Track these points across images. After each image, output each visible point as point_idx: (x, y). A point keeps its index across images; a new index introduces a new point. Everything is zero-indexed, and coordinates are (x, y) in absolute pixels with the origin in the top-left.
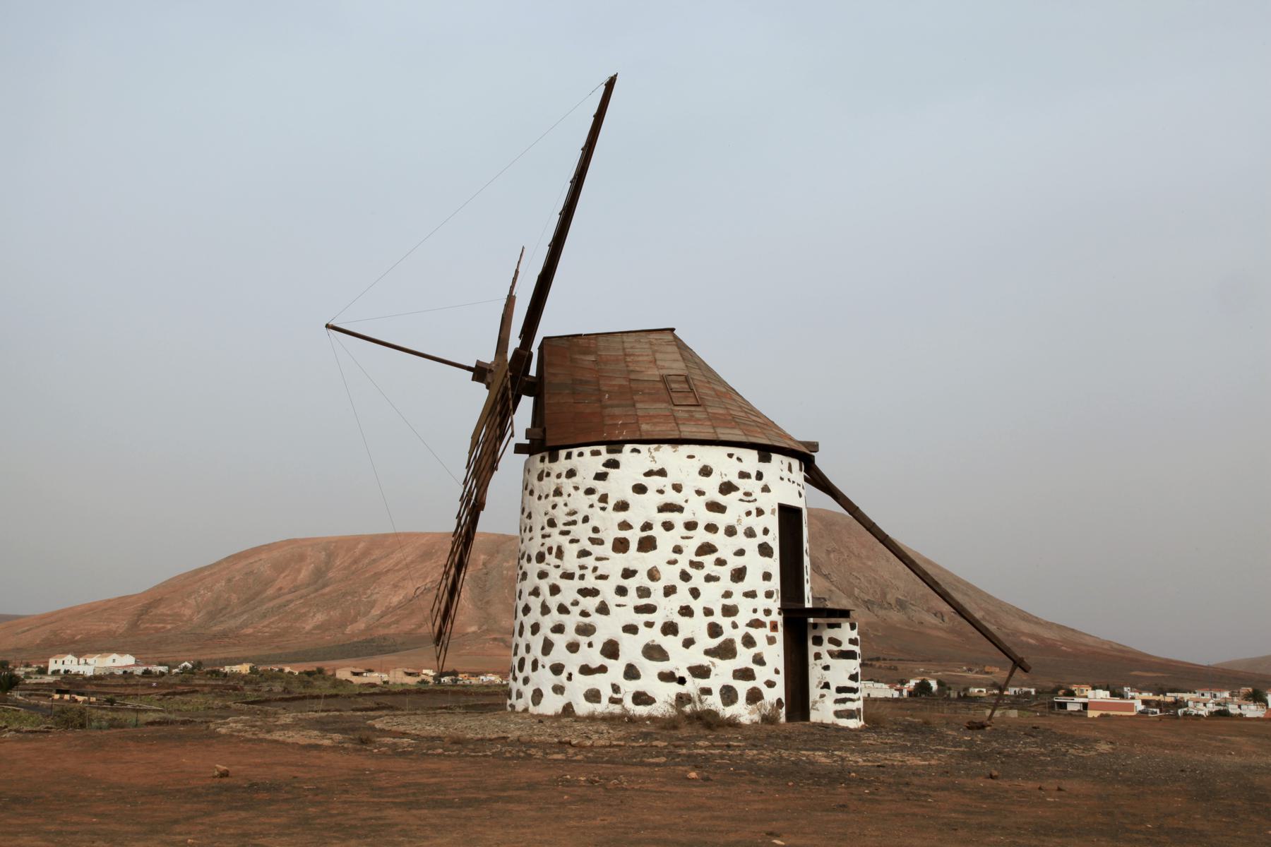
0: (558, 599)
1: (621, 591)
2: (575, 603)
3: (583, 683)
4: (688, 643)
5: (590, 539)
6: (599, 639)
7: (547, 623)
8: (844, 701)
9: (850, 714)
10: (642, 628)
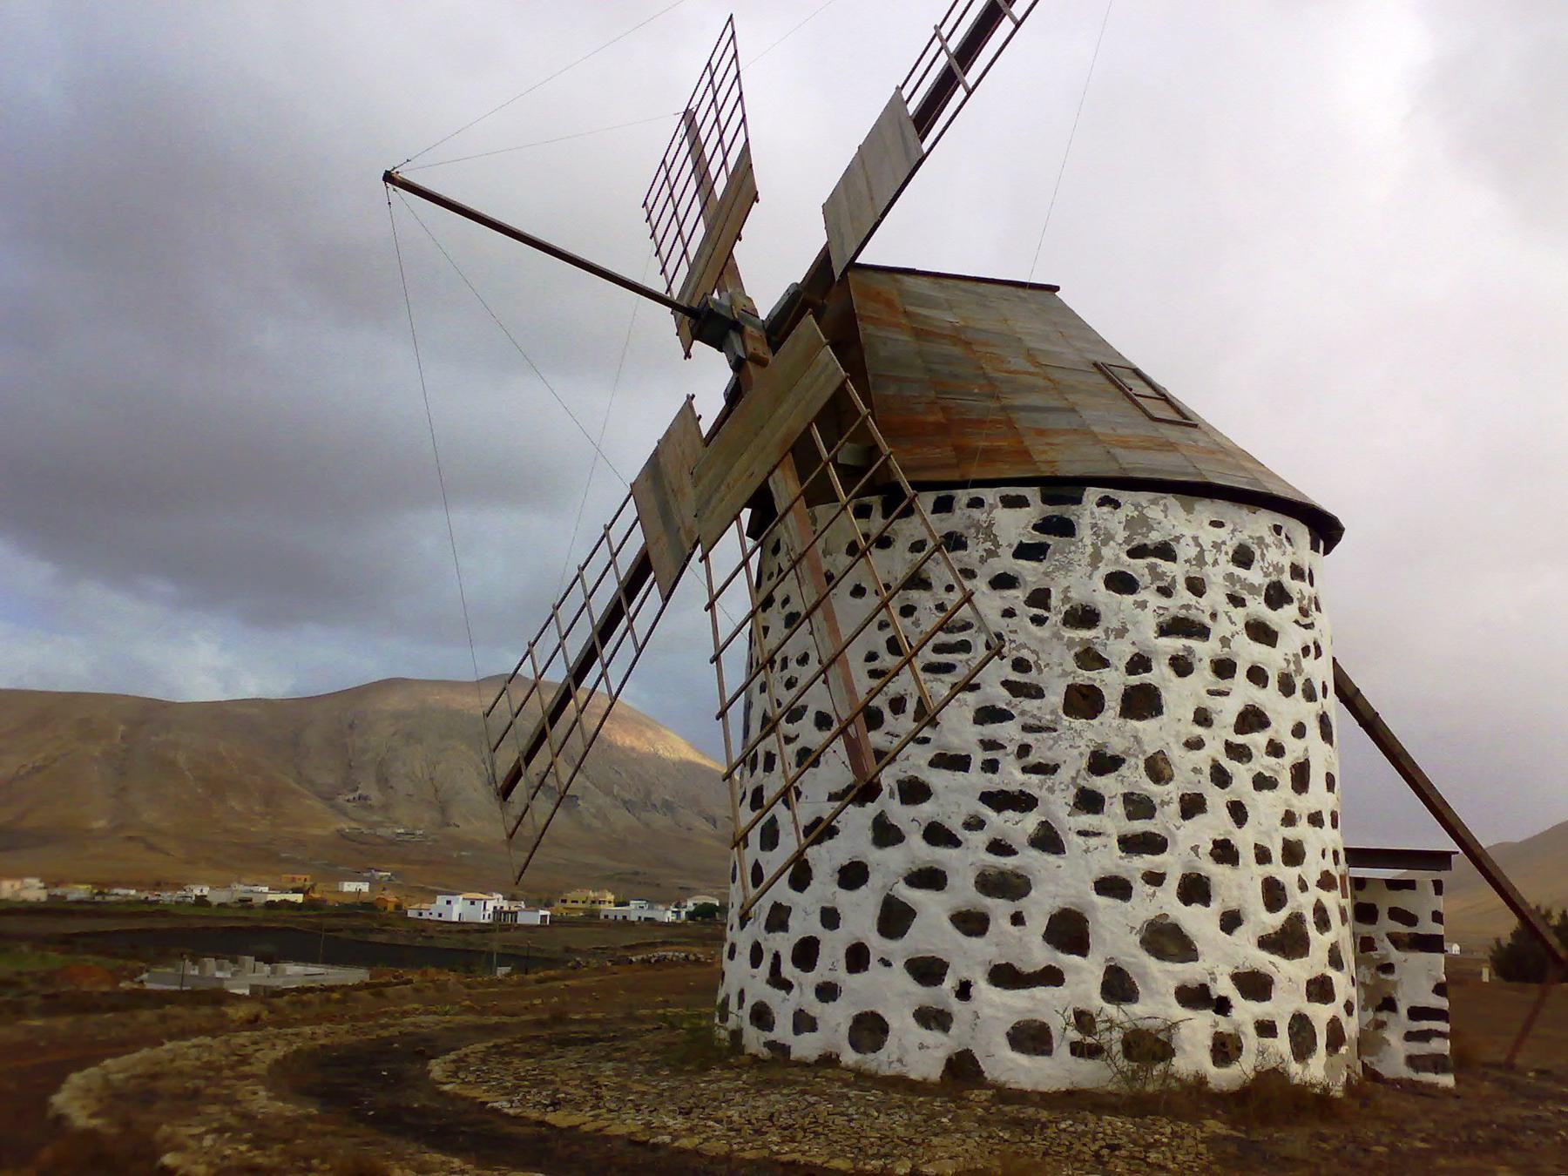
1: (1089, 802)
2: (975, 824)
4: (1231, 921)
5: (1006, 684)
6: (1040, 907)
7: (889, 865)
8: (1425, 1036)
9: (1436, 1063)
10: (1140, 888)
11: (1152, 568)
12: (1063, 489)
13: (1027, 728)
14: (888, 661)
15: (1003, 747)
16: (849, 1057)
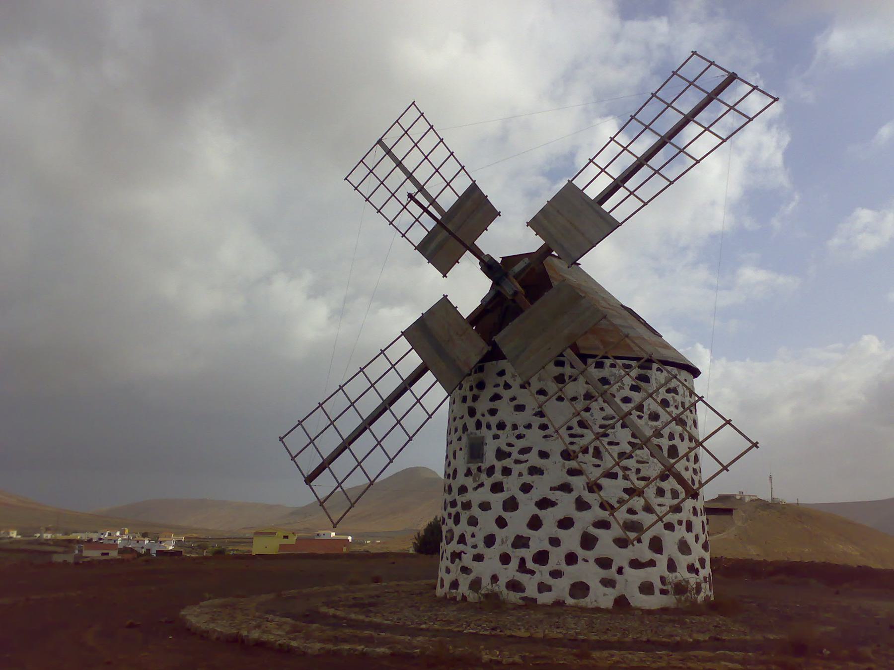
5: (629, 443)
7: (584, 520)
11: (673, 397)
12: (647, 363)
13: (638, 462)
14: (577, 430)
16: (570, 601)
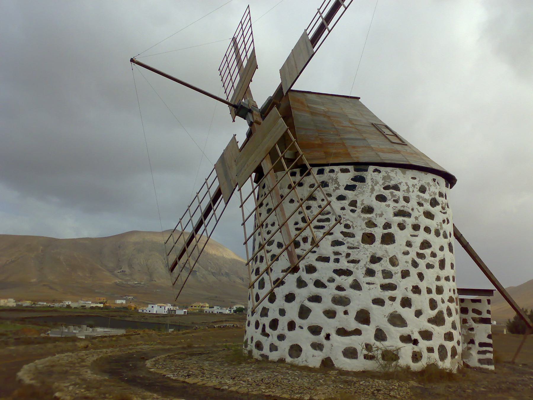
0: (315, 276)
1: (370, 273)
2: (332, 280)
3: (341, 343)
4: (418, 313)
5: (342, 233)
6: (353, 309)
7: (302, 294)
8: (484, 352)
9: (488, 362)
10: (387, 302)
11: (392, 193)
12: (361, 166)
13: (349, 248)
14: (302, 225)
15: (341, 254)
16: (289, 359)
